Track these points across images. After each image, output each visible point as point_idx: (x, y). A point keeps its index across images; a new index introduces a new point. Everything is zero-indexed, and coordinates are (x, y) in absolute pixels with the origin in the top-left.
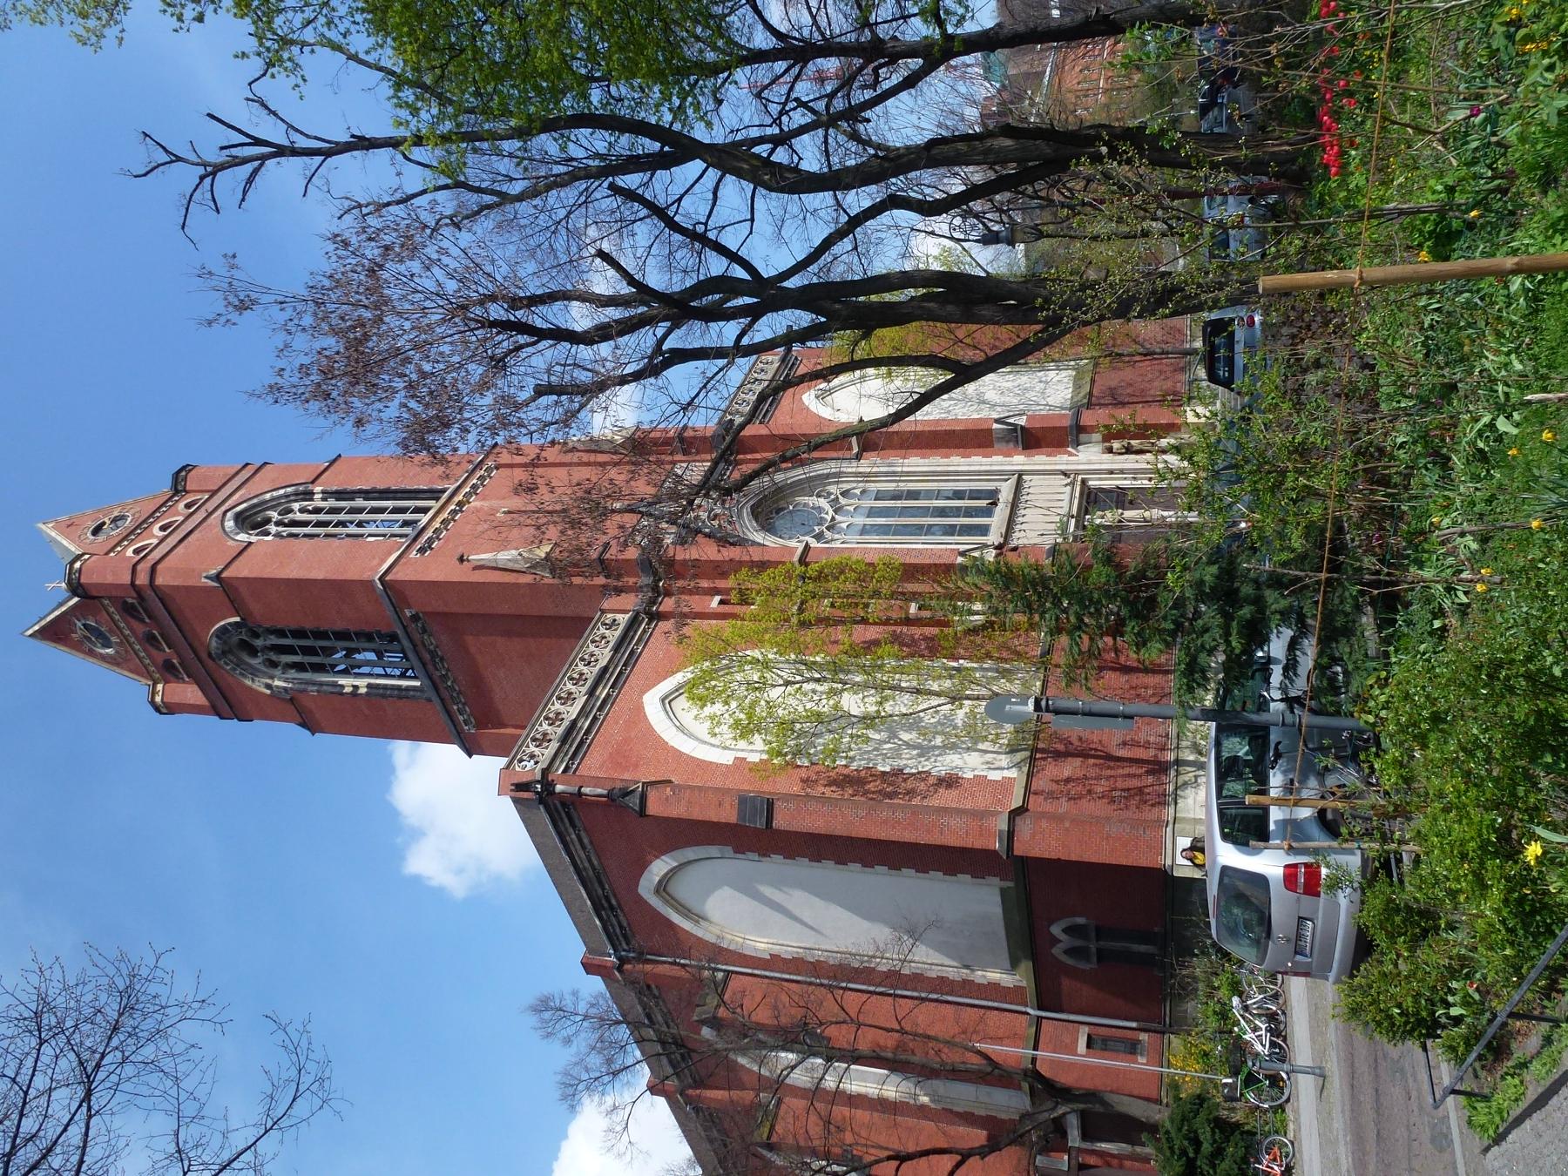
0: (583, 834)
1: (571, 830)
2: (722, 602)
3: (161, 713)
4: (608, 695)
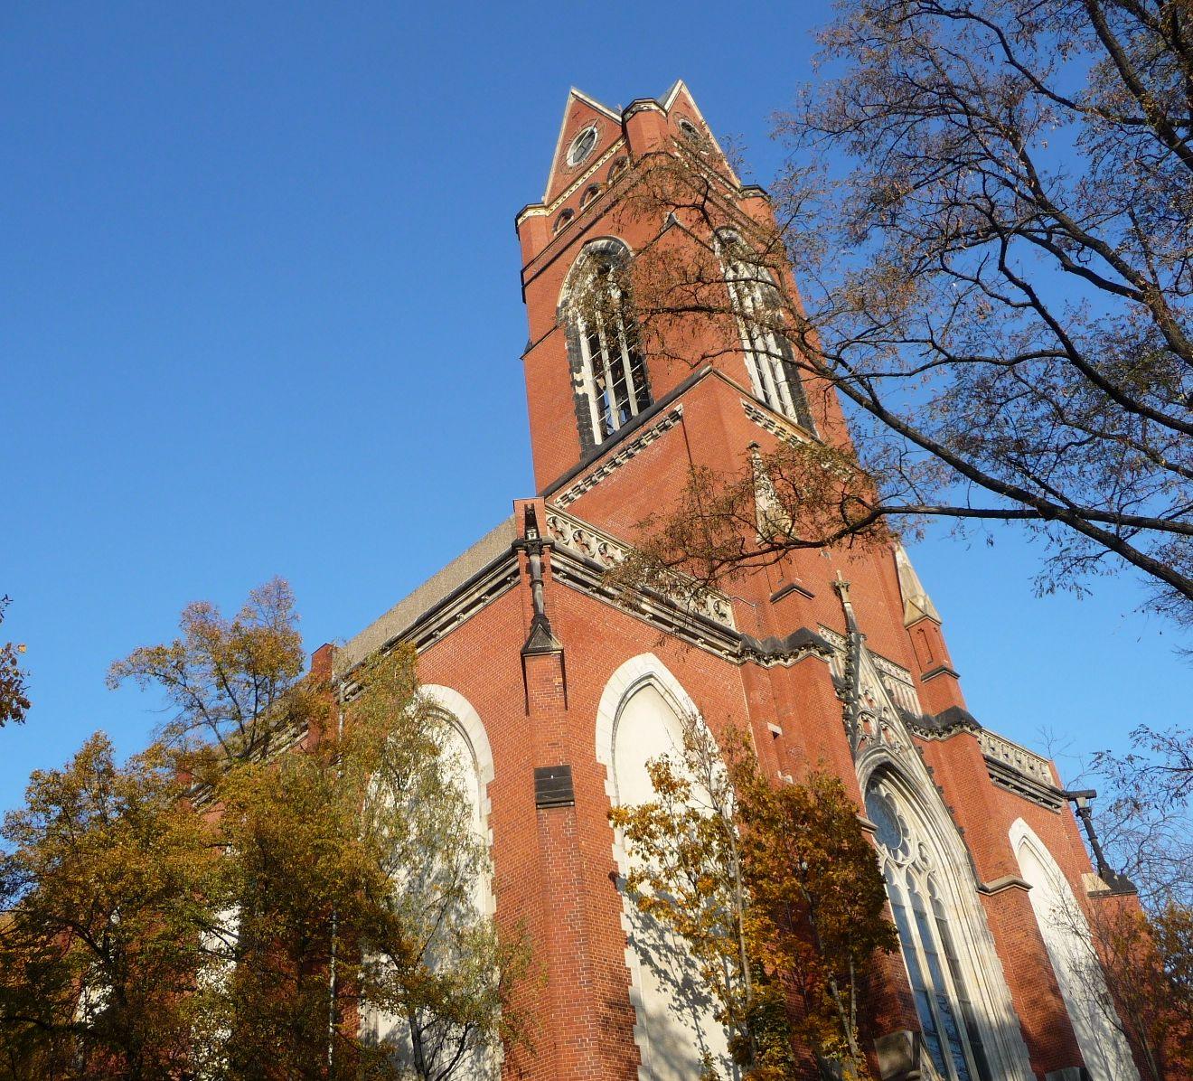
2: (775, 735)
4: (644, 612)
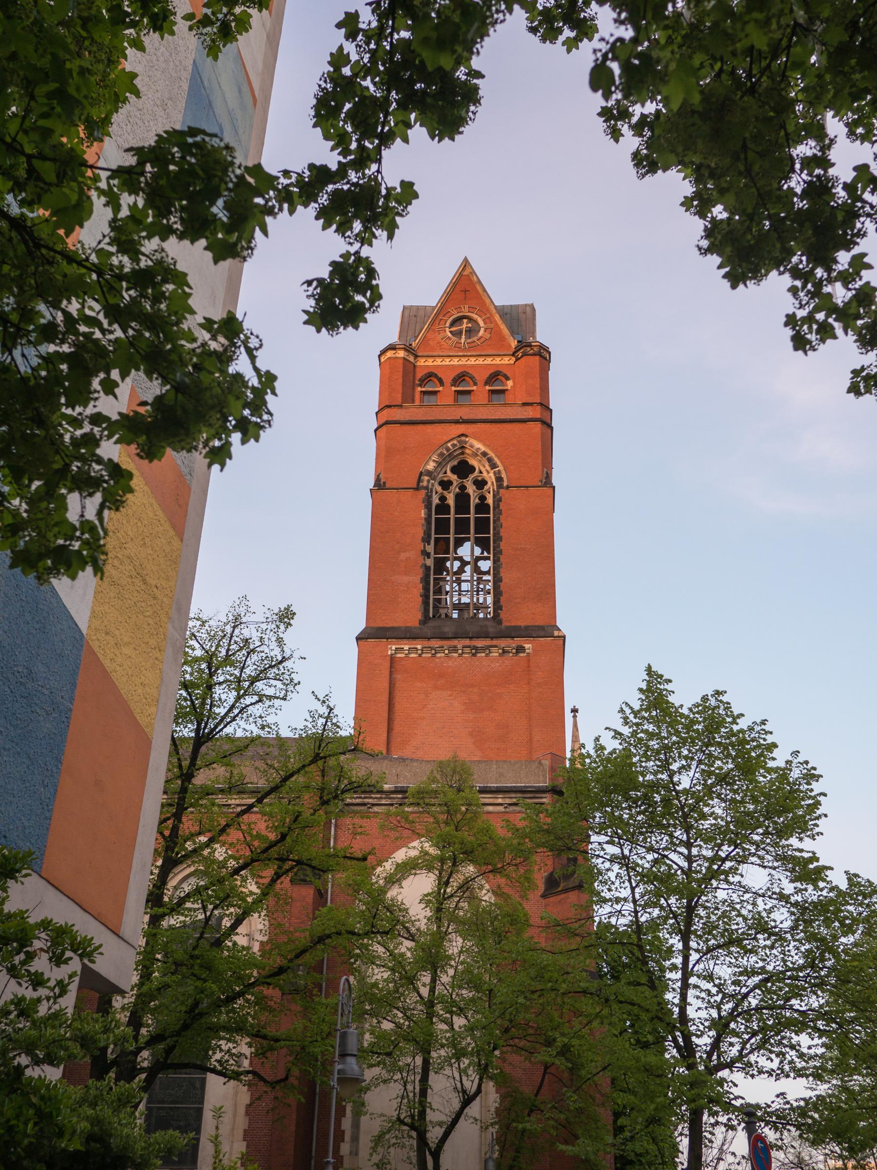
0: (501, 809)
1: (508, 801)
3: (379, 356)
